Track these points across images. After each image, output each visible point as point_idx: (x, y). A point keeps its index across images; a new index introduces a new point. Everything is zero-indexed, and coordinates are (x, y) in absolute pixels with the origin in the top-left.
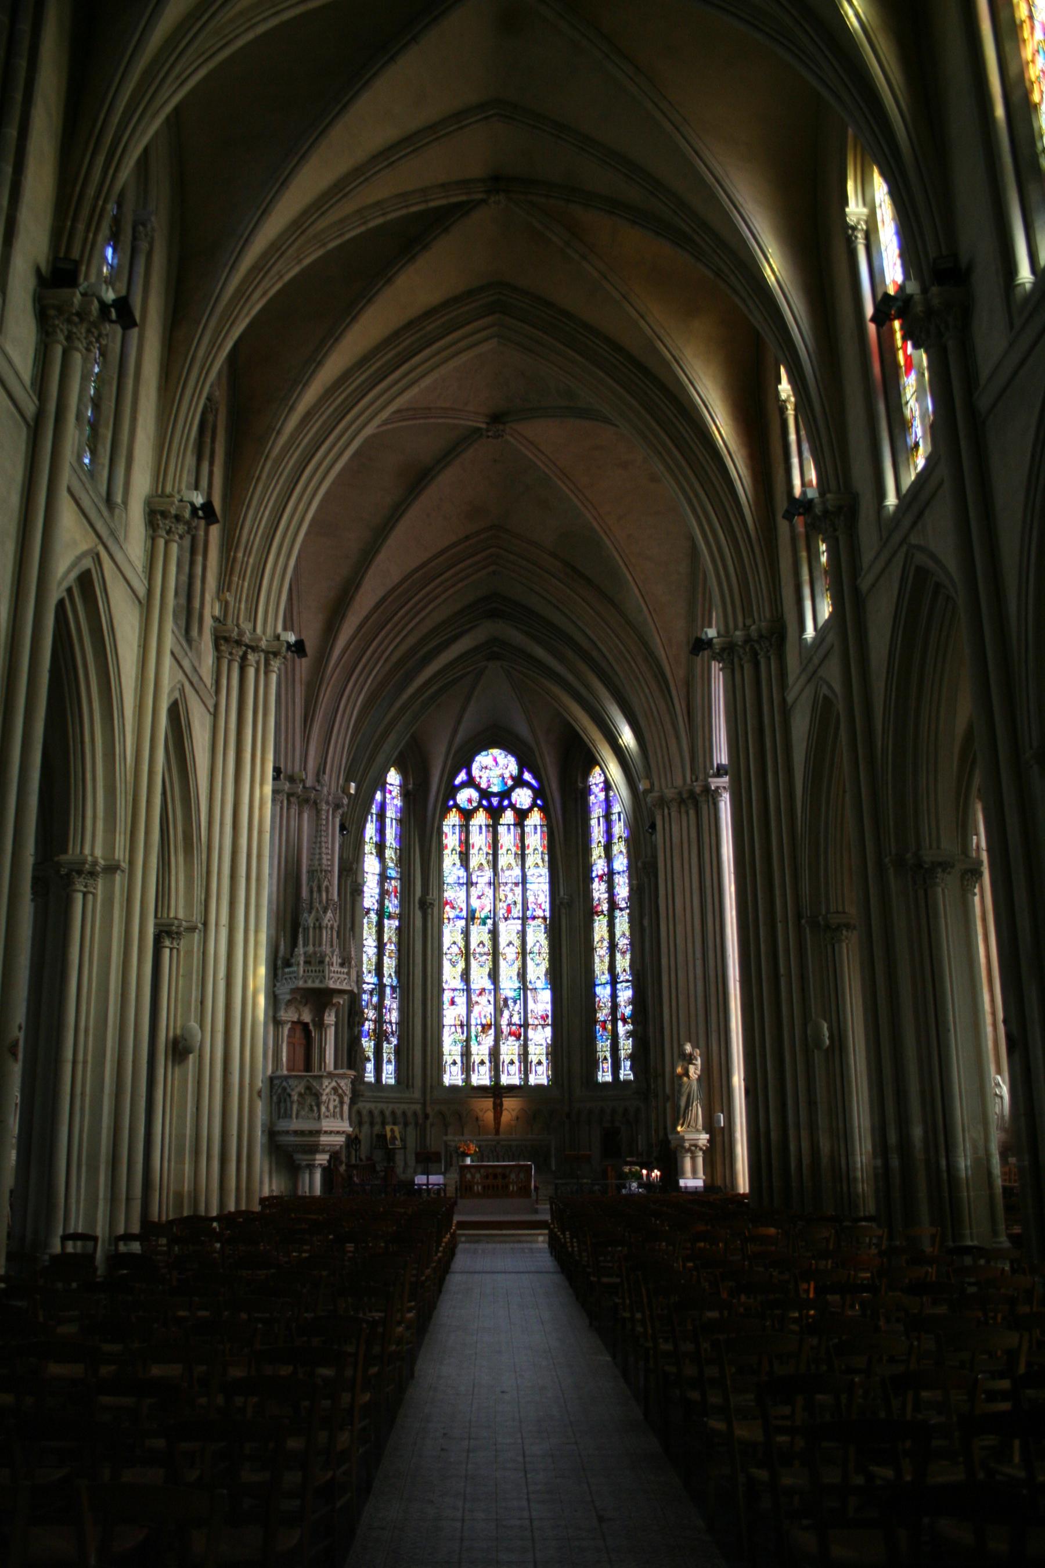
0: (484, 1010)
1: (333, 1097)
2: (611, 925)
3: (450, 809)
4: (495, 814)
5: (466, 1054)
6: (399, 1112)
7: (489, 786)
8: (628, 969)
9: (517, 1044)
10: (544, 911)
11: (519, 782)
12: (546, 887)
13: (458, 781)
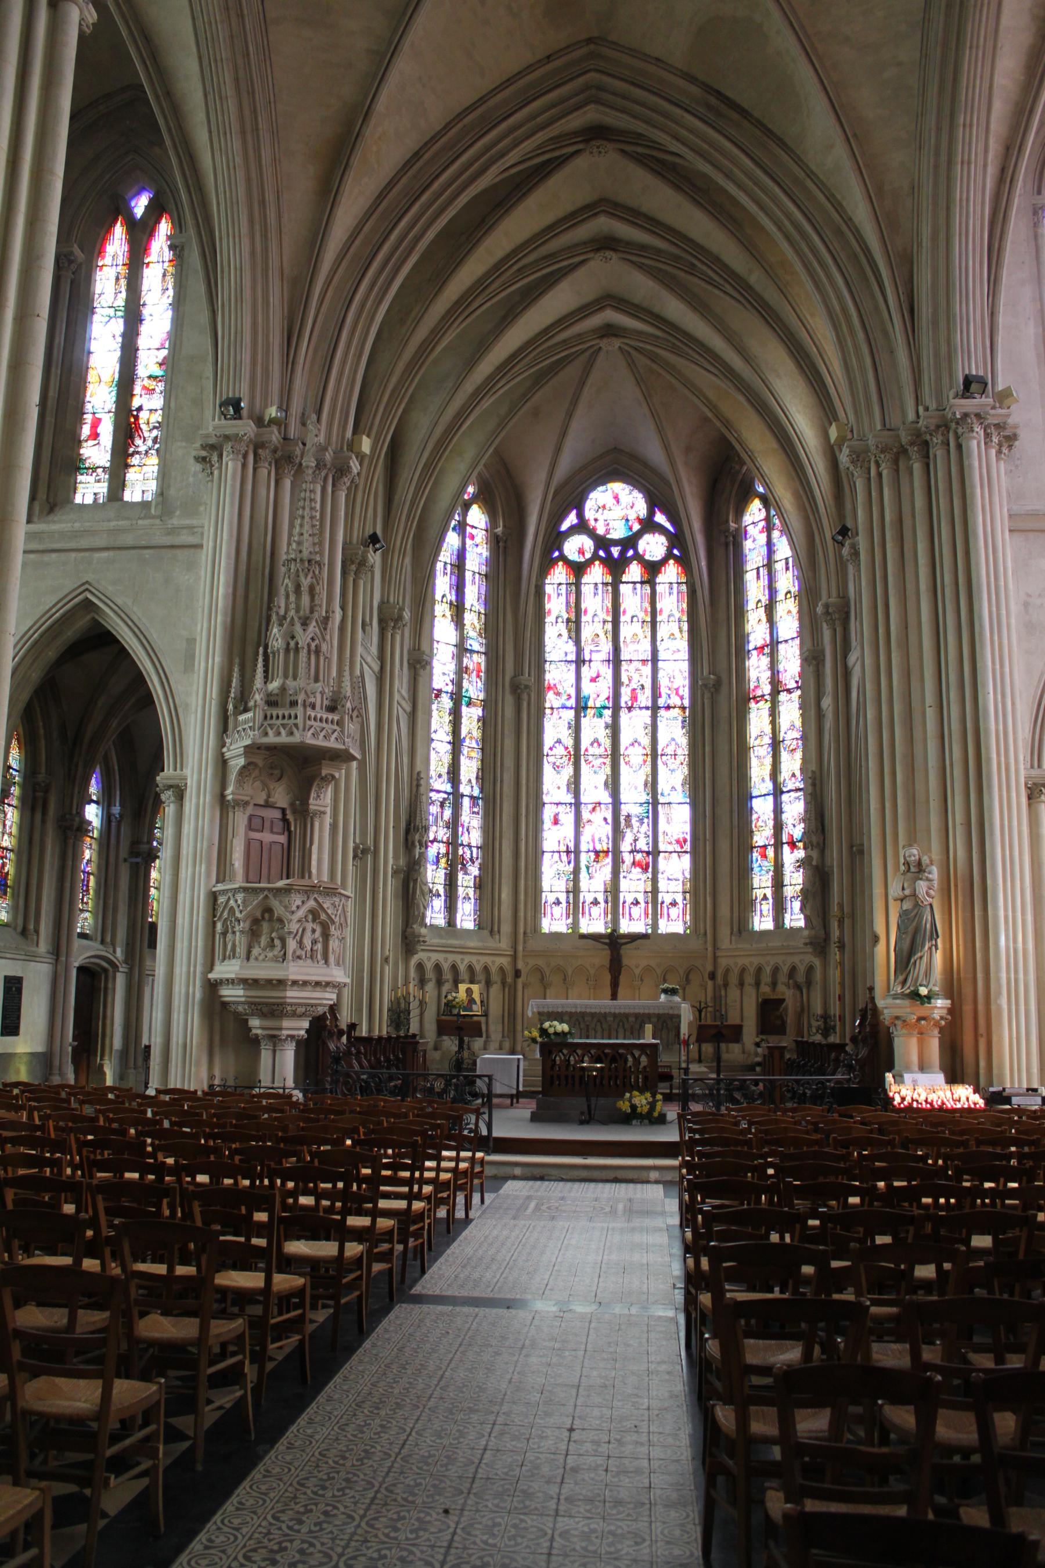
1: (310, 926)
2: (774, 713)
3: (554, 562)
4: (616, 568)
5: (574, 890)
6: (478, 968)
7: (608, 531)
8: (798, 773)
9: (644, 877)
10: (682, 698)
11: (648, 525)
12: (685, 666)
13: (565, 526)
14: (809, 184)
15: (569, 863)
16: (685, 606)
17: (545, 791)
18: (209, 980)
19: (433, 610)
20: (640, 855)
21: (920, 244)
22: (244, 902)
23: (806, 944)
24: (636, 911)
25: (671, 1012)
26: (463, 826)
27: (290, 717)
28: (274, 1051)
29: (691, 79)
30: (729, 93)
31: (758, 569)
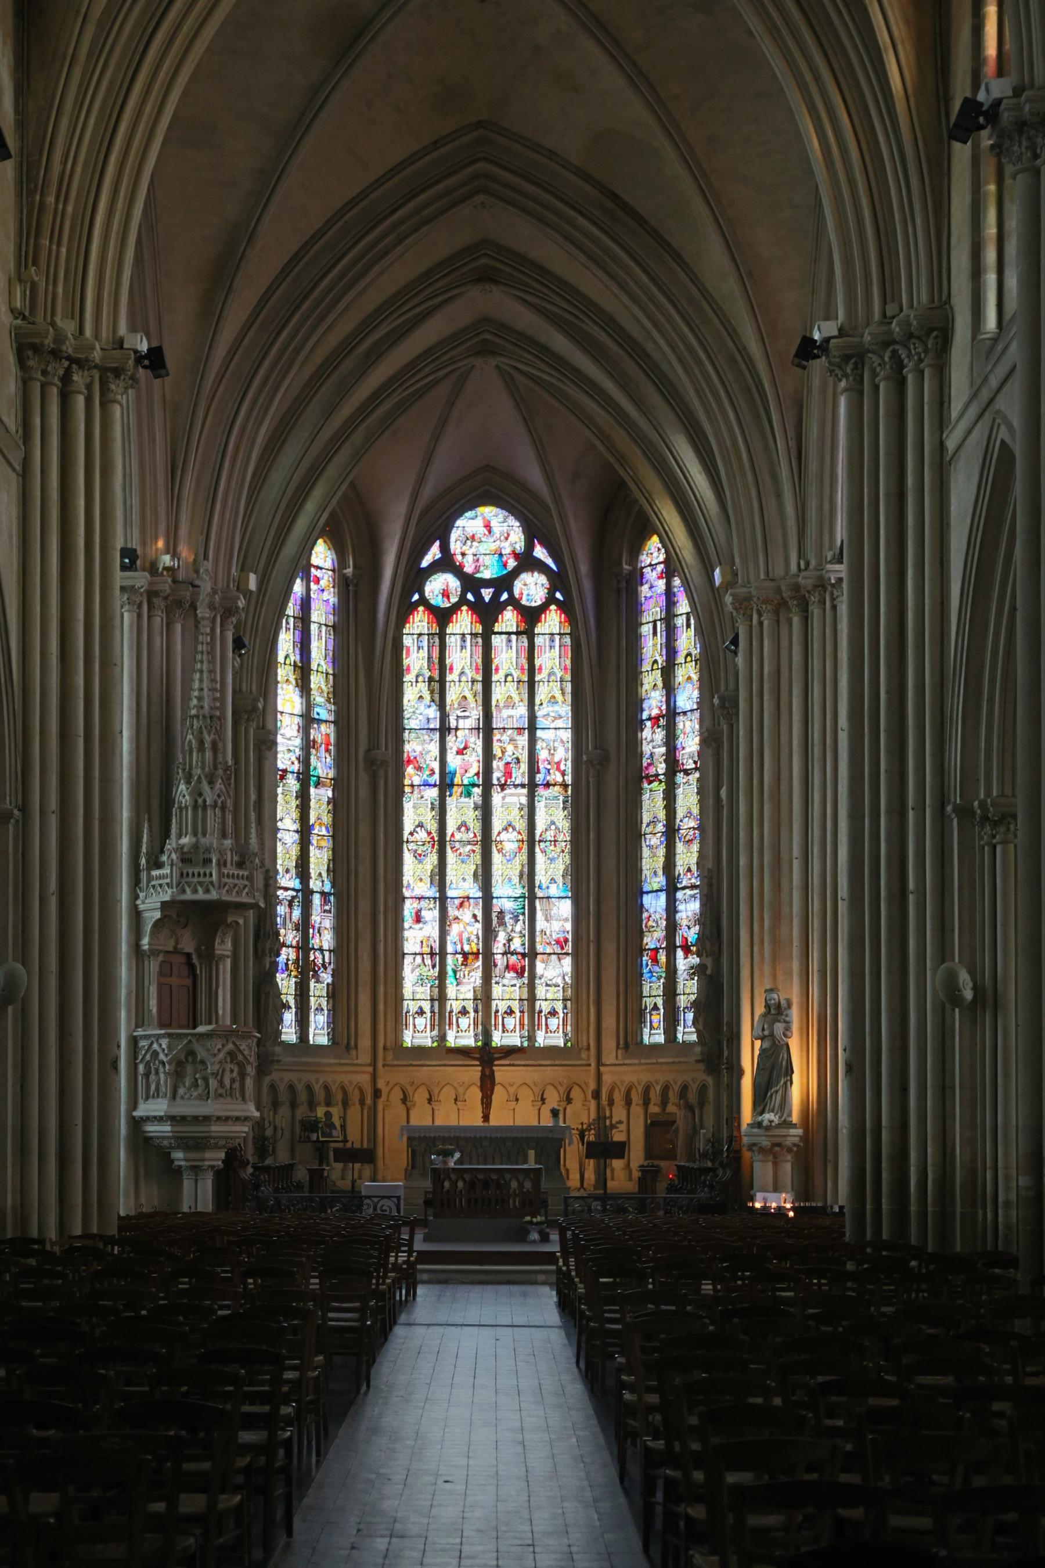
0: (466, 928)
1: (228, 1066)
2: (670, 798)
3: (412, 608)
4: (487, 615)
8: (694, 868)
10: (563, 774)
11: (526, 562)
12: (567, 735)
13: (425, 564)
14: (704, 304)
15: (434, 966)
16: (568, 662)
17: (405, 883)
18: (134, 1118)
19: (276, 675)
20: (515, 957)
21: (810, 390)
22: (169, 1047)
23: (698, 1061)
24: (511, 1022)
25: (550, 1135)
26: (313, 927)
27: (205, 875)
28: (196, 1180)
29: (586, 177)
30: (626, 198)
31: (655, 622)
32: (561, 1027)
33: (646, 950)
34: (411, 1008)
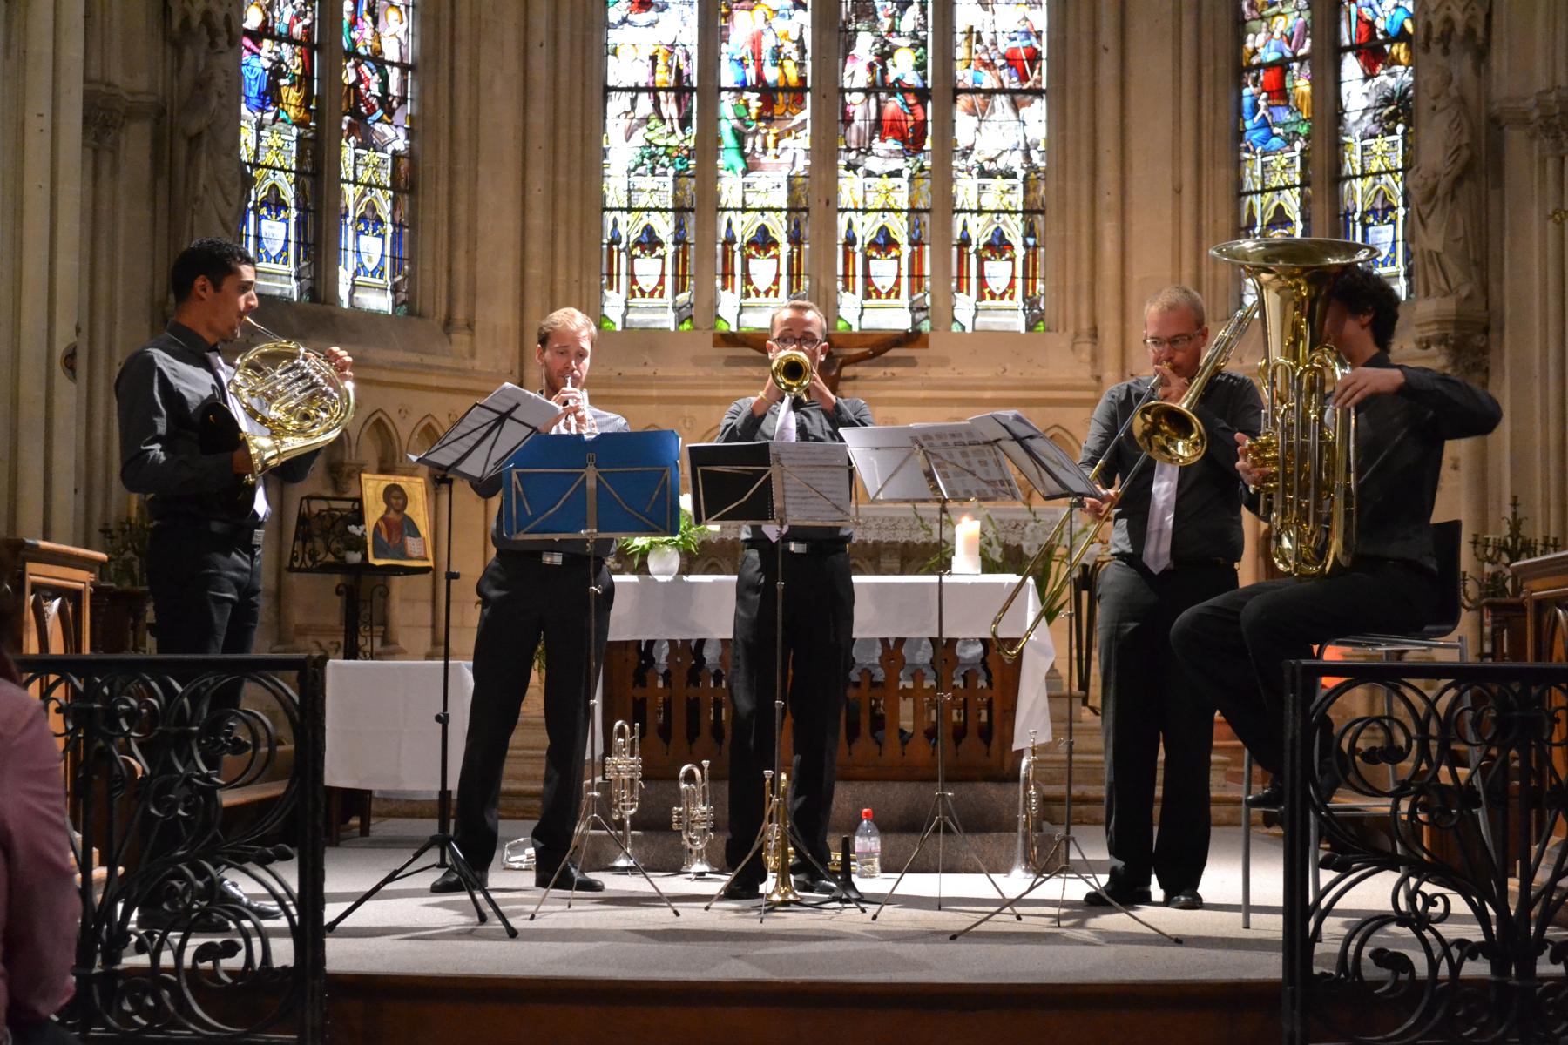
5: (697, 204)
32: (1019, 283)
33: (1250, 68)
34: (622, 229)
